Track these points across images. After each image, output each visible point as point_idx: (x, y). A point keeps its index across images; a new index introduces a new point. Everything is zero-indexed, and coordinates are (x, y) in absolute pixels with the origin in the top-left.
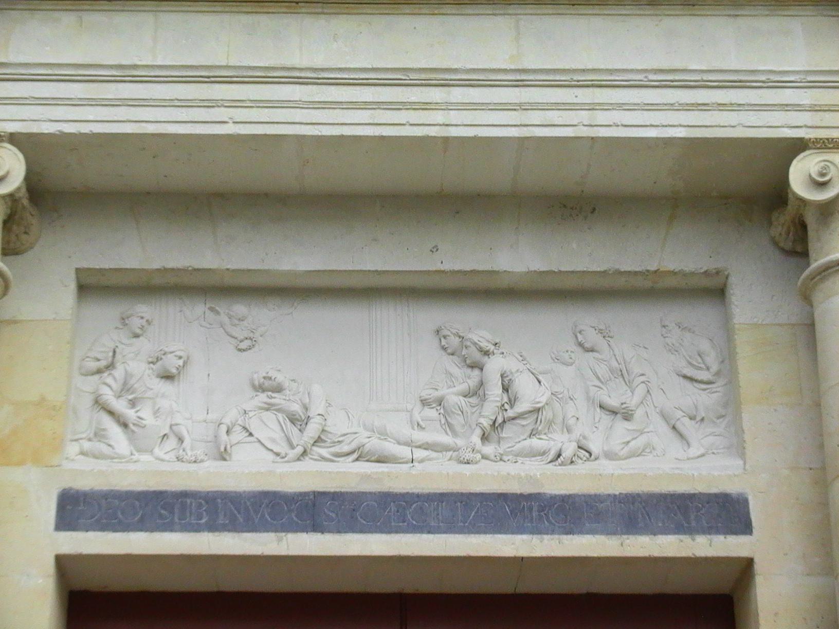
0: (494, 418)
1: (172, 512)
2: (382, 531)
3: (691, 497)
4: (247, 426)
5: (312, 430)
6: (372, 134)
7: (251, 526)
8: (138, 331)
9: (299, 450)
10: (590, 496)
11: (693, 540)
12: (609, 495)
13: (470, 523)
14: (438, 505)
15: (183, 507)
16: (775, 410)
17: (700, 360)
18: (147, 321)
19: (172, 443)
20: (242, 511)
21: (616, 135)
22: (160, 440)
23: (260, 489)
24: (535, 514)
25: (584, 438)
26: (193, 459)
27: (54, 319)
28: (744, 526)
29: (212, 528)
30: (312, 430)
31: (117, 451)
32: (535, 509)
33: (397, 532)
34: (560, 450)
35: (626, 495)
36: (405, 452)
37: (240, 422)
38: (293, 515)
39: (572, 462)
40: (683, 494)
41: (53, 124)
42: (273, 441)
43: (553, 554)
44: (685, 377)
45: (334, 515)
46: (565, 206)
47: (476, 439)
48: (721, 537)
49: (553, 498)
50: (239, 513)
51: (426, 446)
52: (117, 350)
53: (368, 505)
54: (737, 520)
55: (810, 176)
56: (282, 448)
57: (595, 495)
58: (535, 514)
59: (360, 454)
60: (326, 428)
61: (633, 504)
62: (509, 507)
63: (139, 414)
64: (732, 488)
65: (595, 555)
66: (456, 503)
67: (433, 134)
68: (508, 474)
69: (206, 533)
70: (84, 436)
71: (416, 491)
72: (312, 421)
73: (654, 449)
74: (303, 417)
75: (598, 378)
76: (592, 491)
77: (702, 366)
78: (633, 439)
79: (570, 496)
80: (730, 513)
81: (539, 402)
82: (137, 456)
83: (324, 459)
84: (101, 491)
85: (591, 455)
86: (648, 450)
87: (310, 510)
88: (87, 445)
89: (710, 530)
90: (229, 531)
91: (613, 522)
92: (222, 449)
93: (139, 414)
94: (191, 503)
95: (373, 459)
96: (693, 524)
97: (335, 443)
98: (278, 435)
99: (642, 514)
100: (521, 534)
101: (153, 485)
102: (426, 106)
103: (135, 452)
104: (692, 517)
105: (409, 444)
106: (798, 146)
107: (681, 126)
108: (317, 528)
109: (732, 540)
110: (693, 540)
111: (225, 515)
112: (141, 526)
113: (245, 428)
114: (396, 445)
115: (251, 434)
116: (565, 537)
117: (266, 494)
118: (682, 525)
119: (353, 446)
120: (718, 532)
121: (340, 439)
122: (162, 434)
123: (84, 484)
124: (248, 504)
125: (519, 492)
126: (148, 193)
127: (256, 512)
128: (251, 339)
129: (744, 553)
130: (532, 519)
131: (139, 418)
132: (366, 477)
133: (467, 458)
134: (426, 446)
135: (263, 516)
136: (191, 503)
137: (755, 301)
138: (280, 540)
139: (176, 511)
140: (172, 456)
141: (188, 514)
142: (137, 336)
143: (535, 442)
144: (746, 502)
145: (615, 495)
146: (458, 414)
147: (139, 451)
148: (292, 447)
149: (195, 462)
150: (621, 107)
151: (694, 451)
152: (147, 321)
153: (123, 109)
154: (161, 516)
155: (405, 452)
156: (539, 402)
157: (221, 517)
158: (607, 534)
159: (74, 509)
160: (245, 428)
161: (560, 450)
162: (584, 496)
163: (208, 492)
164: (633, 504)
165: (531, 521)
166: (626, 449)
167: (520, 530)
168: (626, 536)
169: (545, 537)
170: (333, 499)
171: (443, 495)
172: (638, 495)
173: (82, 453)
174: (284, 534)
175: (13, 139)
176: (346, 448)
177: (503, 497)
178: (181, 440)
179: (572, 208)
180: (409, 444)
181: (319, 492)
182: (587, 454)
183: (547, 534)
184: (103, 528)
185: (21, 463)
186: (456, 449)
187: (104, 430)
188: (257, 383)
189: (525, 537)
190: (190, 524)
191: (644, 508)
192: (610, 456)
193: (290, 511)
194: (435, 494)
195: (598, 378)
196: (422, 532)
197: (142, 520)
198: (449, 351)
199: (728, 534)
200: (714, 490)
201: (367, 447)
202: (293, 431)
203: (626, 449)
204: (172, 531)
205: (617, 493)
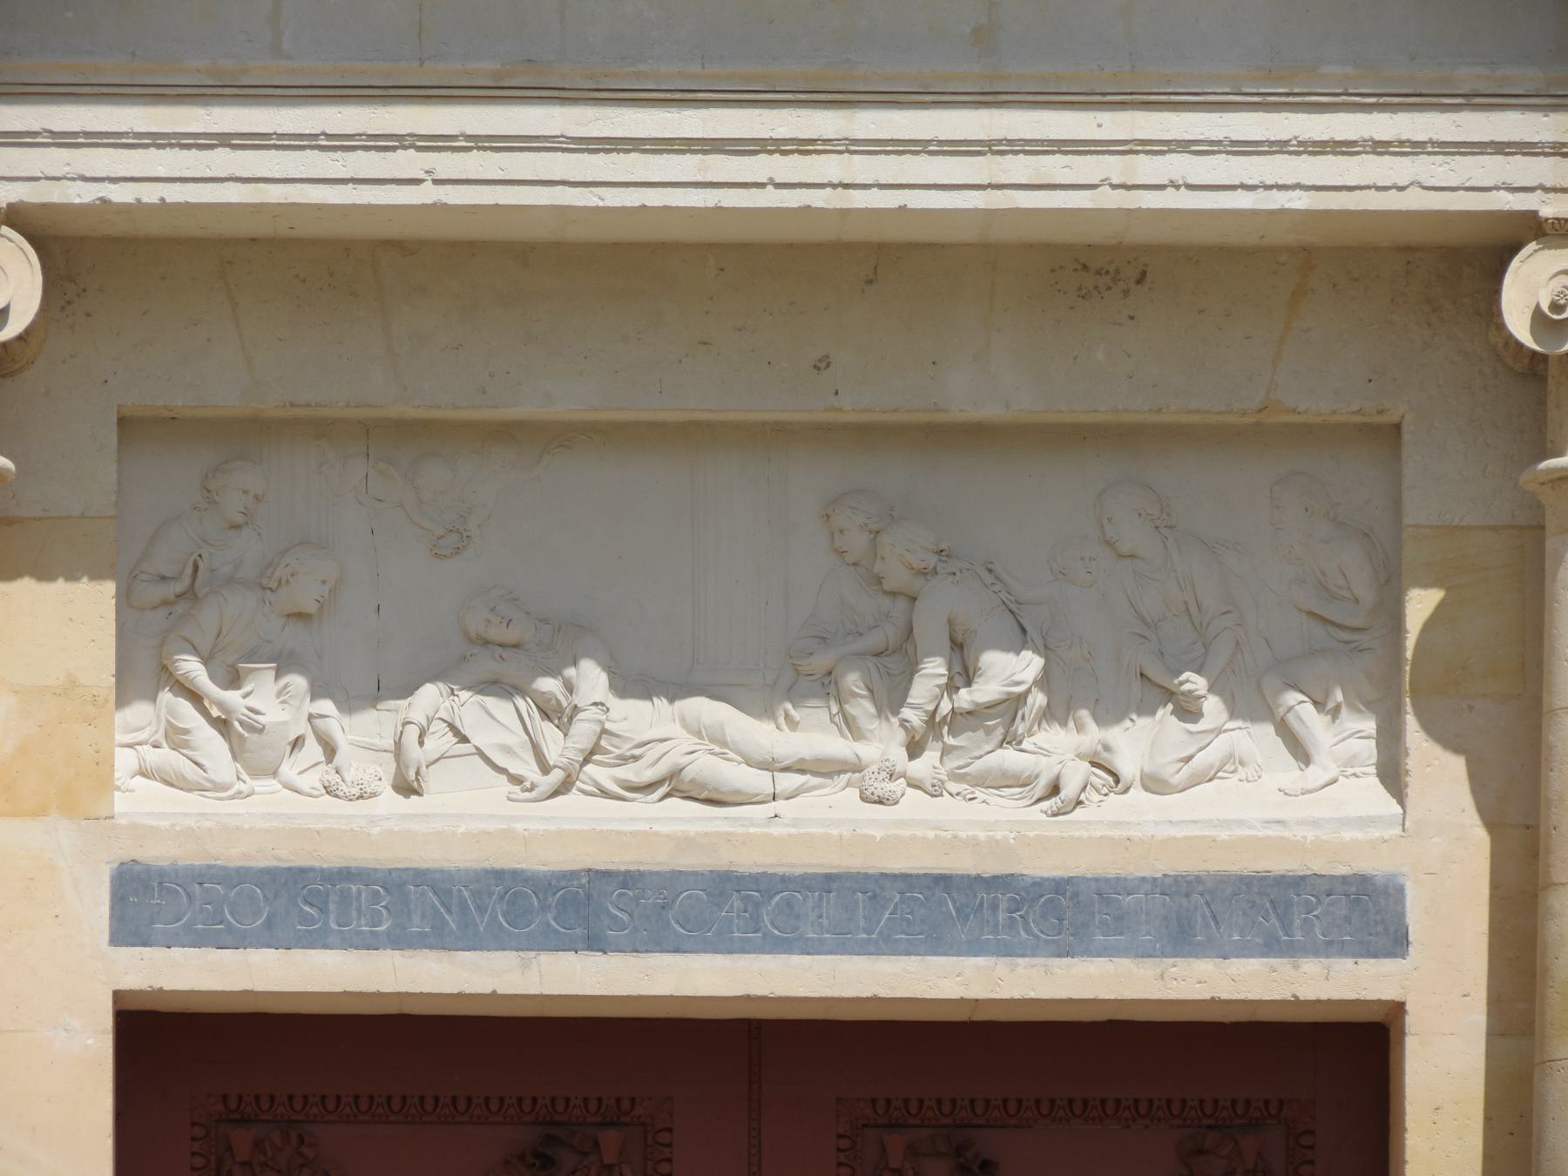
0: (931, 708)
1: (323, 910)
2: (716, 950)
3: (1298, 882)
4: (458, 724)
5: (584, 731)
6: (702, 205)
7: (469, 939)
8: (239, 519)
9: (556, 776)
10: (1107, 880)
11: (1296, 967)
12: (1144, 879)
13: (880, 933)
14: (821, 898)
15: (345, 898)
16: (1471, 708)
17: (1341, 582)
18: (256, 497)
19: (313, 750)
20: (454, 909)
21: (1174, 206)
22: (289, 748)
23: (487, 865)
24: (1002, 916)
25: (1107, 748)
26: (356, 791)
27: (83, 516)
28: (1397, 943)
29: (400, 941)
30: (584, 731)
31: (212, 775)
32: (1003, 906)
33: (743, 951)
34: (1058, 778)
35: (1176, 877)
36: (759, 781)
37: (442, 714)
38: (550, 917)
39: (1079, 803)
40: (1283, 877)
41: (90, 185)
42: (507, 750)
43: (1032, 995)
44: (1310, 613)
45: (624, 917)
46: (1085, 267)
47: (899, 754)
48: (1348, 963)
49: (1039, 884)
50: (449, 911)
51: (799, 768)
52: (201, 564)
53: (689, 897)
54: (1380, 928)
55: (1538, 307)
56: (531, 771)
57: (1118, 879)
58: (1002, 916)
59: (675, 785)
60: (608, 726)
61: (1187, 896)
62: (954, 901)
63: (250, 702)
64: (1373, 865)
65: (1112, 997)
66: (854, 892)
67: (819, 204)
68: (955, 837)
69: (389, 951)
70: (142, 736)
71: (780, 870)
72: (581, 716)
73: (1242, 763)
74: (565, 704)
75: (1143, 620)
76: (1112, 872)
77: (1346, 594)
78: (1201, 749)
79: (1069, 880)
80: (1366, 911)
81: (1018, 683)
82: (251, 784)
83: (605, 793)
84: (191, 868)
85: (1117, 781)
86: (1229, 767)
87: (581, 905)
88: (152, 756)
89: (1330, 948)
90: (431, 947)
91: (1149, 934)
92: (412, 775)
93: (250, 702)
94: (359, 892)
95: (702, 796)
96: (1299, 937)
97: (624, 760)
98: (517, 739)
99: (1204, 916)
100: (976, 955)
101: (287, 855)
102: (803, 147)
103: (245, 776)
104: (1298, 922)
105: (769, 765)
106: (1526, 230)
107: (1298, 186)
108: (594, 943)
109: (1369, 966)
110: (1296, 967)
111: (423, 916)
112: (270, 937)
113: (452, 727)
114: (744, 766)
115: (464, 739)
116: (1057, 961)
117: (498, 875)
118: (1278, 940)
119: (661, 769)
120: (1342, 950)
121: (637, 752)
122: (292, 737)
123: (157, 853)
124: (466, 894)
125: (973, 872)
126: (254, 240)
127: (481, 910)
128: (458, 531)
129: (1388, 993)
130: (997, 925)
131: (251, 710)
132: (685, 842)
133: (879, 792)
134: (799, 768)
135: (494, 918)
136: (359, 892)
137: (1444, 483)
138: (525, 966)
139: (332, 907)
140: (311, 781)
141: (354, 914)
142: (237, 527)
143: (1008, 758)
144: (1401, 890)
145: (1155, 879)
146: (863, 697)
147: (256, 772)
148: (545, 769)
149: (361, 797)
150: (1183, 146)
151: (1316, 774)
152: (256, 497)
153: (222, 153)
154: (306, 919)
155: (759, 781)
156: (1018, 683)
157: (416, 919)
158: (1137, 956)
159: (145, 900)
160: (452, 727)
161: (1058, 778)
162: (1097, 880)
163: (390, 871)
164: (1187, 896)
165: (995, 931)
166: (1187, 770)
167: (975, 948)
168: (1170, 961)
169: (1020, 960)
170: (625, 886)
171: (829, 878)
172: (1199, 879)
173: (143, 773)
174: (532, 954)
175: (15, 217)
176: (649, 775)
177: (943, 881)
178: (330, 750)
179: (1098, 273)
180: (769, 765)
181: (597, 871)
182: (1110, 779)
183: (1023, 956)
184: (199, 941)
185: (38, 812)
186: (857, 767)
187: (186, 732)
188: (473, 633)
189: (981, 961)
190: (359, 933)
191: (1207, 903)
192: (1154, 784)
193: (544, 908)
194: (815, 876)
195: (1143, 620)
196: (790, 952)
197: (269, 924)
198: (850, 558)
199: (1362, 956)
200: (1342, 870)
201: (689, 773)
202: (549, 733)
203: (1187, 770)
204: (325, 947)
205: (1159, 875)
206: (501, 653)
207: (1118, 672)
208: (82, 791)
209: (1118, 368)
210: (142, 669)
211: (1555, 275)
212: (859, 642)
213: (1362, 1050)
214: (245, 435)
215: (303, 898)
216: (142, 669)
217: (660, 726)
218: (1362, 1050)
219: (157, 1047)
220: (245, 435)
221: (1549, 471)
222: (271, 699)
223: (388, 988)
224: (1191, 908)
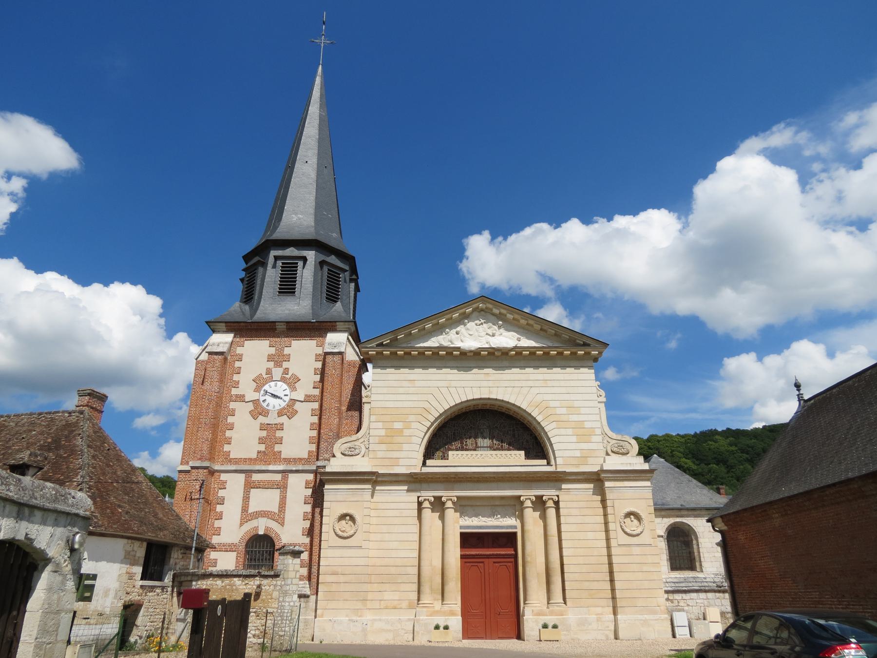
80: (515, 527)
87: (481, 527)
159: (461, 527)
206: (476, 516)
207: (503, 516)
208: (458, 522)
209: (503, 502)
210: (461, 517)
211: (638, 535)
212: (492, 515)
213: (515, 534)
214: (465, 506)
215: (468, 527)
216: (461, 517)
217: (484, 519)
218: (515, 534)
219: (462, 534)
220: (465, 506)
221: (420, 347)
222: (466, 518)
223: (347, 641)
224: (508, 527)
